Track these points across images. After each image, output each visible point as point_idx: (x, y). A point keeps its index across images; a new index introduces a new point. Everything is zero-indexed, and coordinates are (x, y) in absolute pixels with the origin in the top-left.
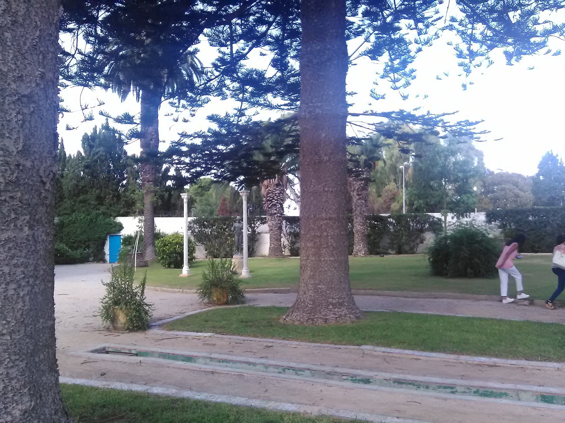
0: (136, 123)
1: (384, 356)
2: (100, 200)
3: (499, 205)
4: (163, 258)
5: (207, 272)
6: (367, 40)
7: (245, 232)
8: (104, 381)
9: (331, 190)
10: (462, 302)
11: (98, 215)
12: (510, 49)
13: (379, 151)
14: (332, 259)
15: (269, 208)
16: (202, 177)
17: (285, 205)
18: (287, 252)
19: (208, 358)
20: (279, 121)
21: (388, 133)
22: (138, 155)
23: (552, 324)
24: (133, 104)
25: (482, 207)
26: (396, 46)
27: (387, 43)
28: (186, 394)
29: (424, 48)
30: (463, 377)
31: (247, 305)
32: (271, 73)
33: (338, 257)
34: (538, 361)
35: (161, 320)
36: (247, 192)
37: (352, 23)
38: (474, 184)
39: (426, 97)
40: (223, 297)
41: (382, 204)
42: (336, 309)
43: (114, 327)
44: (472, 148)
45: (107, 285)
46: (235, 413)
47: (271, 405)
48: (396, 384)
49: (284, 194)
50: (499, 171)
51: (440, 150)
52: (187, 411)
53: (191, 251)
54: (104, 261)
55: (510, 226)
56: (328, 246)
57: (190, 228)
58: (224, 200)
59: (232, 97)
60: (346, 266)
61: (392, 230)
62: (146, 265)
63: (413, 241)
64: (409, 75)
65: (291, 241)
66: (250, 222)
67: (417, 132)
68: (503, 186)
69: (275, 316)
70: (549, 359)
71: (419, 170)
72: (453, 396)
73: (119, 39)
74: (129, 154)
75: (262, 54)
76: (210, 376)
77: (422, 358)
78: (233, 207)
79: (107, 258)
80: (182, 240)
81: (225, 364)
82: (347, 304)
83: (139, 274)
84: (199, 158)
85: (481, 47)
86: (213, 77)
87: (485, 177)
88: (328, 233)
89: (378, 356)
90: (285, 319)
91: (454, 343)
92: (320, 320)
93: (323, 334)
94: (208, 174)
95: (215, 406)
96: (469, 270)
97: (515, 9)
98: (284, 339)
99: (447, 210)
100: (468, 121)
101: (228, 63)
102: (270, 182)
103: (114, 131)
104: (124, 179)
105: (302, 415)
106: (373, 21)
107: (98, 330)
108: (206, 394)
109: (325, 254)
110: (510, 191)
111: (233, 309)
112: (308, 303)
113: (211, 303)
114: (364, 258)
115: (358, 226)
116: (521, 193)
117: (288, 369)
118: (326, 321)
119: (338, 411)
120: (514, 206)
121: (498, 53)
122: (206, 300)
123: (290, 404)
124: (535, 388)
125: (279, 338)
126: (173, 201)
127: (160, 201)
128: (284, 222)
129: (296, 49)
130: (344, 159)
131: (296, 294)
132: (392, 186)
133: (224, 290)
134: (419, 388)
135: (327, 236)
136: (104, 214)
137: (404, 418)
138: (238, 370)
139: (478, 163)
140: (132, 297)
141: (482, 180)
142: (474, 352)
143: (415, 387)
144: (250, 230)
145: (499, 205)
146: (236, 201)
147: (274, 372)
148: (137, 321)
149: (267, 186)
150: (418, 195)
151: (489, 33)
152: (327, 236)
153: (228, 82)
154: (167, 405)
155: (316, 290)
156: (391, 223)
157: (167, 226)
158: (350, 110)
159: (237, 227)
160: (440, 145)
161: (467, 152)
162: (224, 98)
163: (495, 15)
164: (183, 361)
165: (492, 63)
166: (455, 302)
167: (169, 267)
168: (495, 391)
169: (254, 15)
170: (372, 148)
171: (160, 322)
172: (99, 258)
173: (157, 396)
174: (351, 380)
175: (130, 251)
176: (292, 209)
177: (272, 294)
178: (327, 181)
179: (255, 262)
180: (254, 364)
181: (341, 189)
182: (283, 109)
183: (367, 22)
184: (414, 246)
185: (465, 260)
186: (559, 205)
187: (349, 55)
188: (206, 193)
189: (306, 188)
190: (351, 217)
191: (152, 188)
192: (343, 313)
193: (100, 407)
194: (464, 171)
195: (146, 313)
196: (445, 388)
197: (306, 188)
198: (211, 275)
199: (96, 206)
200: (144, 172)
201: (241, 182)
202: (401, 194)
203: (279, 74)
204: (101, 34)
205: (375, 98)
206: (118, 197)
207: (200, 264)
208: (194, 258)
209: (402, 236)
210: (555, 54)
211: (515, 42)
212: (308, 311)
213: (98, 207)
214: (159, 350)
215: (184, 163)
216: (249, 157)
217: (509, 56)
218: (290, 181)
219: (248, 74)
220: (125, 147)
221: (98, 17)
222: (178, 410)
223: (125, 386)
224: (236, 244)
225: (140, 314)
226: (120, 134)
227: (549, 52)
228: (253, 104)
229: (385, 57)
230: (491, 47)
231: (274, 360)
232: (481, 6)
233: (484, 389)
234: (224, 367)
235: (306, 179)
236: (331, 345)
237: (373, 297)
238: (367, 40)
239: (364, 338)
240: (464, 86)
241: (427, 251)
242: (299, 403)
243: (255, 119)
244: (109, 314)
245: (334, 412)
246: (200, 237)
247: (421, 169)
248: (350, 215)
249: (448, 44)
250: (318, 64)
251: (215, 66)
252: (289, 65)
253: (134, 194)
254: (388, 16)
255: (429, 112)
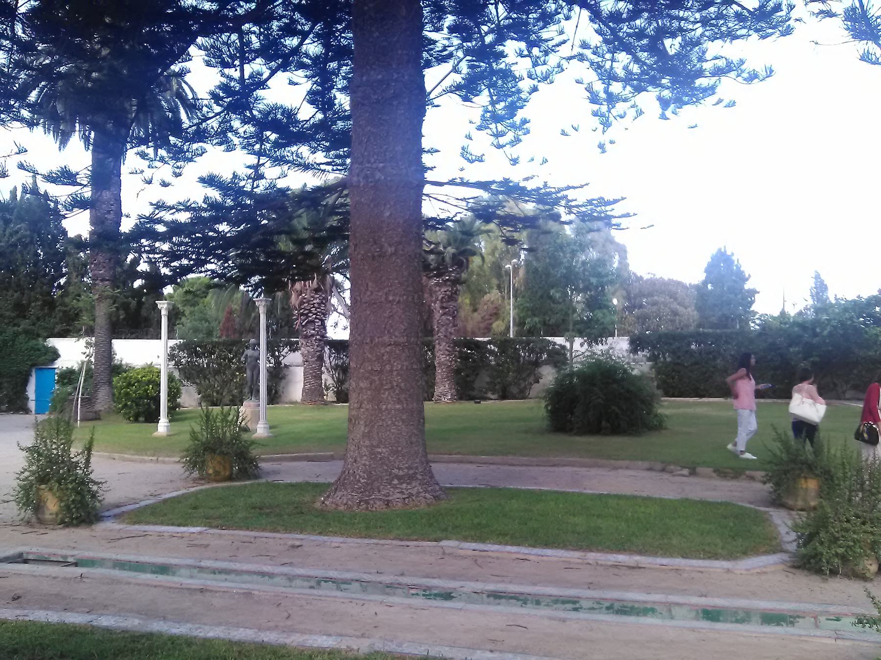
0: (81, 184)
1: (474, 556)
2: (21, 309)
3: (649, 326)
4: (125, 406)
5: (197, 428)
6: (455, 70)
7: (264, 364)
8: (17, 608)
9: (397, 299)
10: (594, 471)
11: (16, 335)
12: (667, 94)
13: (474, 242)
14: (398, 406)
15: (303, 326)
16: (191, 276)
17: (329, 322)
18: (330, 396)
19: (195, 567)
20: (318, 190)
21: (484, 213)
22: (85, 235)
23: (721, 504)
24: (78, 155)
25: (624, 329)
26: (500, 82)
27: (484, 74)
28: (157, 626)
29: (541, 86)
30: (590, 586)
31: (263, 481)
32: (307, 113)
33: (407, 404)
34: (700, 558)
35: (118, 506)
36: (266, 301)
37: (435, 42)
38: (614, 294)
39: (545, 161)
40: (225, 468)
41: (479, 322)
42: (404, 486)
43: (38, 519)
44: (612, 241)
45: (28, 450)
46: (236, 654)
47: (294, 640)
48: (492, 599)
49: (328, 304)
50: (649, 277)
51: (565, 242)
52: (157, 653)
53: (173, 395)
54: (27, 411)
55: (665, 358)
56: (392, 387)
57: (171, 357)
58: (231, 312)
59: (244, 148)
60: (420, 416)
61: (493, 363)
62: (96, 417)
63: (524, 380)
64: (520, 128)
65: (338, 378)
66: (272, 347)
67: (531, 214)
68: (656, 298)
69: (307, 498)
70: (715, 556)
71: (533, 272)
72: (574, 615)
73: (55, 46)
74: (71, 235)
75: (291, 83)
76: (199, 596)
77: (531, 558)
78: (244, 324)
79: (32, 405)
80: (159, 376)
81: (224, 576)
82: (420, 477)
83: (81, 432)
84: (186, 244)
85: (624, 87)
86: (211, 115)
87: (629, 285)
88: (392, 366)
89: (464, 557)
90: (323, 503)
91: (579, 534)
92: (378, 503)
93: (383, 525)
94: (201, 272)
95: (203, 645)
96: (604, 423)
97: (673, 35)
98: (320, 533)
99: (573, 334)
100: (603, 199)
101: (237, 93)
102: (305, 285)
103: (46, 196)
104: (62, 276)
105: (343, 653)
106: (464, 40)
107: (11, 525)
108: (189, 625)
109: (387, 399)
110: (665, 306)
111: (240, 487)
112: (360, 477)
113: (204, 478)
114: (451, 406)
115: (442, 356)
116: (680, 309)
117: (326, 582)
118: (388, 503)
119: (400, 645)
120: (671, 328)
121: (648, 99)
122: (196, 474)
123: (325, 637)
124: (695, 600)
125: (313, 532)
126: (144, 313)
127: (121, 312)
128: (327, 349)
129: (344, 78)
130: (418, 251)
131: (342, 463)
132: (493, 295)
133: (225, 457)
134: (525, 603)
135: (391, 371)
136: (26, 332)
137: (501, 651)
138: (243, 586)
139: (620, 263)
140: (69, 470)
141: (624, 289)
142: (608, 547)
143: (520, 603)
144: (272, 361)
145: (649, 326)
146: (250, 315)
147: (303, 587)
148: (78, 509)
149: (299, 292)
150: (532, 310)
151: (635, 68)
152: (391, 371)
153: (236, 124)
154: (123, 645)
155: (373, 455)
156: (492, 352)
157: (133, 353)
158: (429, 176)
159: (250, 357)
160: (565, 234)
161: (604, 246)
162: (230, 149)
163: (645, 41)
164: (153, 572)
165: (640, 114)
166: (583, 471)
167: (136, 420)
168: (636, 605)
169: (278, 20)
170: (465, 235)
171: (117, 511)
172: (17, 405)
173: (108, 630)
174: (424, 595)
175: (70, 394)
176: (338, 328)
177: (305, 463)
178: (391, 286)
179: (280, 411)
180: (271, 575)
181: (413, 299)
182: (324, 171)
183: (456, 42)
184: (525, 388)
185: (600, 409)
186: (734, 327)
187: (428, 88)
188: (202, 301)
189: (360, 295)
190: (431, 342)
191: (109, 291)
192: (414, 492)
193: (9, 652)
194: (599, 275)
195: (94, 496)
196: (564, 602)
197: (360, 295)
198: (205, 433)
199: (14, 319)
200: (95, 265)
201: (256, 286)
202: (508, 307)
203: (320, 116)
204: (23, 35)
205: (468, 160)
206: (51, 304)
207: (189, 415)
208: (179, 406)
209: (509, 372)
210: (728, 106)
211: (673, 82)
212: (360, 488)
213: (16, 321)
214: (114, 557)
215: (161, 252)
216: (268, 246)
217: (664, 103)
218: (338, 286)
219: (269, 113)
220: (65, 223)
221: (17, 8)
222: (143, 652)
223: (53, 617)
224: (249, 384)
225: (83, 497)
226: (56, 202)
227: (720, 101)
228: (279, 161)
229: (483, 98)
230: (639, 89)
231: (302, 567)
232: (625, 28)
233: (621, 604)
234: (221, 581)
235: (360, 282)
236: (395, 542)
237: (462, 465)
238: (455, 70)
239: (446, 530)
240: (601, 146)
241: (544, 394)
242: (341, 635)
243: (281, 184)
244: (29, 498)
245: (394, 646)
246: (190, 373)
247: (536, 271)
248: (429, 338)
249: (578, 82)
250: (378, 101)
251: (215, 97)
252: (336, 102)
253: (78, 300)
254: (487, 34)
255: (546, 183)
